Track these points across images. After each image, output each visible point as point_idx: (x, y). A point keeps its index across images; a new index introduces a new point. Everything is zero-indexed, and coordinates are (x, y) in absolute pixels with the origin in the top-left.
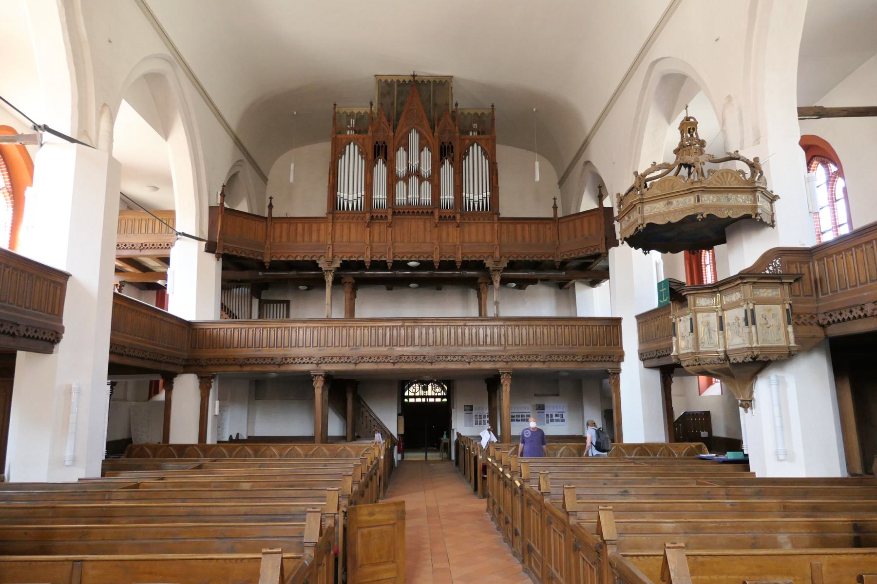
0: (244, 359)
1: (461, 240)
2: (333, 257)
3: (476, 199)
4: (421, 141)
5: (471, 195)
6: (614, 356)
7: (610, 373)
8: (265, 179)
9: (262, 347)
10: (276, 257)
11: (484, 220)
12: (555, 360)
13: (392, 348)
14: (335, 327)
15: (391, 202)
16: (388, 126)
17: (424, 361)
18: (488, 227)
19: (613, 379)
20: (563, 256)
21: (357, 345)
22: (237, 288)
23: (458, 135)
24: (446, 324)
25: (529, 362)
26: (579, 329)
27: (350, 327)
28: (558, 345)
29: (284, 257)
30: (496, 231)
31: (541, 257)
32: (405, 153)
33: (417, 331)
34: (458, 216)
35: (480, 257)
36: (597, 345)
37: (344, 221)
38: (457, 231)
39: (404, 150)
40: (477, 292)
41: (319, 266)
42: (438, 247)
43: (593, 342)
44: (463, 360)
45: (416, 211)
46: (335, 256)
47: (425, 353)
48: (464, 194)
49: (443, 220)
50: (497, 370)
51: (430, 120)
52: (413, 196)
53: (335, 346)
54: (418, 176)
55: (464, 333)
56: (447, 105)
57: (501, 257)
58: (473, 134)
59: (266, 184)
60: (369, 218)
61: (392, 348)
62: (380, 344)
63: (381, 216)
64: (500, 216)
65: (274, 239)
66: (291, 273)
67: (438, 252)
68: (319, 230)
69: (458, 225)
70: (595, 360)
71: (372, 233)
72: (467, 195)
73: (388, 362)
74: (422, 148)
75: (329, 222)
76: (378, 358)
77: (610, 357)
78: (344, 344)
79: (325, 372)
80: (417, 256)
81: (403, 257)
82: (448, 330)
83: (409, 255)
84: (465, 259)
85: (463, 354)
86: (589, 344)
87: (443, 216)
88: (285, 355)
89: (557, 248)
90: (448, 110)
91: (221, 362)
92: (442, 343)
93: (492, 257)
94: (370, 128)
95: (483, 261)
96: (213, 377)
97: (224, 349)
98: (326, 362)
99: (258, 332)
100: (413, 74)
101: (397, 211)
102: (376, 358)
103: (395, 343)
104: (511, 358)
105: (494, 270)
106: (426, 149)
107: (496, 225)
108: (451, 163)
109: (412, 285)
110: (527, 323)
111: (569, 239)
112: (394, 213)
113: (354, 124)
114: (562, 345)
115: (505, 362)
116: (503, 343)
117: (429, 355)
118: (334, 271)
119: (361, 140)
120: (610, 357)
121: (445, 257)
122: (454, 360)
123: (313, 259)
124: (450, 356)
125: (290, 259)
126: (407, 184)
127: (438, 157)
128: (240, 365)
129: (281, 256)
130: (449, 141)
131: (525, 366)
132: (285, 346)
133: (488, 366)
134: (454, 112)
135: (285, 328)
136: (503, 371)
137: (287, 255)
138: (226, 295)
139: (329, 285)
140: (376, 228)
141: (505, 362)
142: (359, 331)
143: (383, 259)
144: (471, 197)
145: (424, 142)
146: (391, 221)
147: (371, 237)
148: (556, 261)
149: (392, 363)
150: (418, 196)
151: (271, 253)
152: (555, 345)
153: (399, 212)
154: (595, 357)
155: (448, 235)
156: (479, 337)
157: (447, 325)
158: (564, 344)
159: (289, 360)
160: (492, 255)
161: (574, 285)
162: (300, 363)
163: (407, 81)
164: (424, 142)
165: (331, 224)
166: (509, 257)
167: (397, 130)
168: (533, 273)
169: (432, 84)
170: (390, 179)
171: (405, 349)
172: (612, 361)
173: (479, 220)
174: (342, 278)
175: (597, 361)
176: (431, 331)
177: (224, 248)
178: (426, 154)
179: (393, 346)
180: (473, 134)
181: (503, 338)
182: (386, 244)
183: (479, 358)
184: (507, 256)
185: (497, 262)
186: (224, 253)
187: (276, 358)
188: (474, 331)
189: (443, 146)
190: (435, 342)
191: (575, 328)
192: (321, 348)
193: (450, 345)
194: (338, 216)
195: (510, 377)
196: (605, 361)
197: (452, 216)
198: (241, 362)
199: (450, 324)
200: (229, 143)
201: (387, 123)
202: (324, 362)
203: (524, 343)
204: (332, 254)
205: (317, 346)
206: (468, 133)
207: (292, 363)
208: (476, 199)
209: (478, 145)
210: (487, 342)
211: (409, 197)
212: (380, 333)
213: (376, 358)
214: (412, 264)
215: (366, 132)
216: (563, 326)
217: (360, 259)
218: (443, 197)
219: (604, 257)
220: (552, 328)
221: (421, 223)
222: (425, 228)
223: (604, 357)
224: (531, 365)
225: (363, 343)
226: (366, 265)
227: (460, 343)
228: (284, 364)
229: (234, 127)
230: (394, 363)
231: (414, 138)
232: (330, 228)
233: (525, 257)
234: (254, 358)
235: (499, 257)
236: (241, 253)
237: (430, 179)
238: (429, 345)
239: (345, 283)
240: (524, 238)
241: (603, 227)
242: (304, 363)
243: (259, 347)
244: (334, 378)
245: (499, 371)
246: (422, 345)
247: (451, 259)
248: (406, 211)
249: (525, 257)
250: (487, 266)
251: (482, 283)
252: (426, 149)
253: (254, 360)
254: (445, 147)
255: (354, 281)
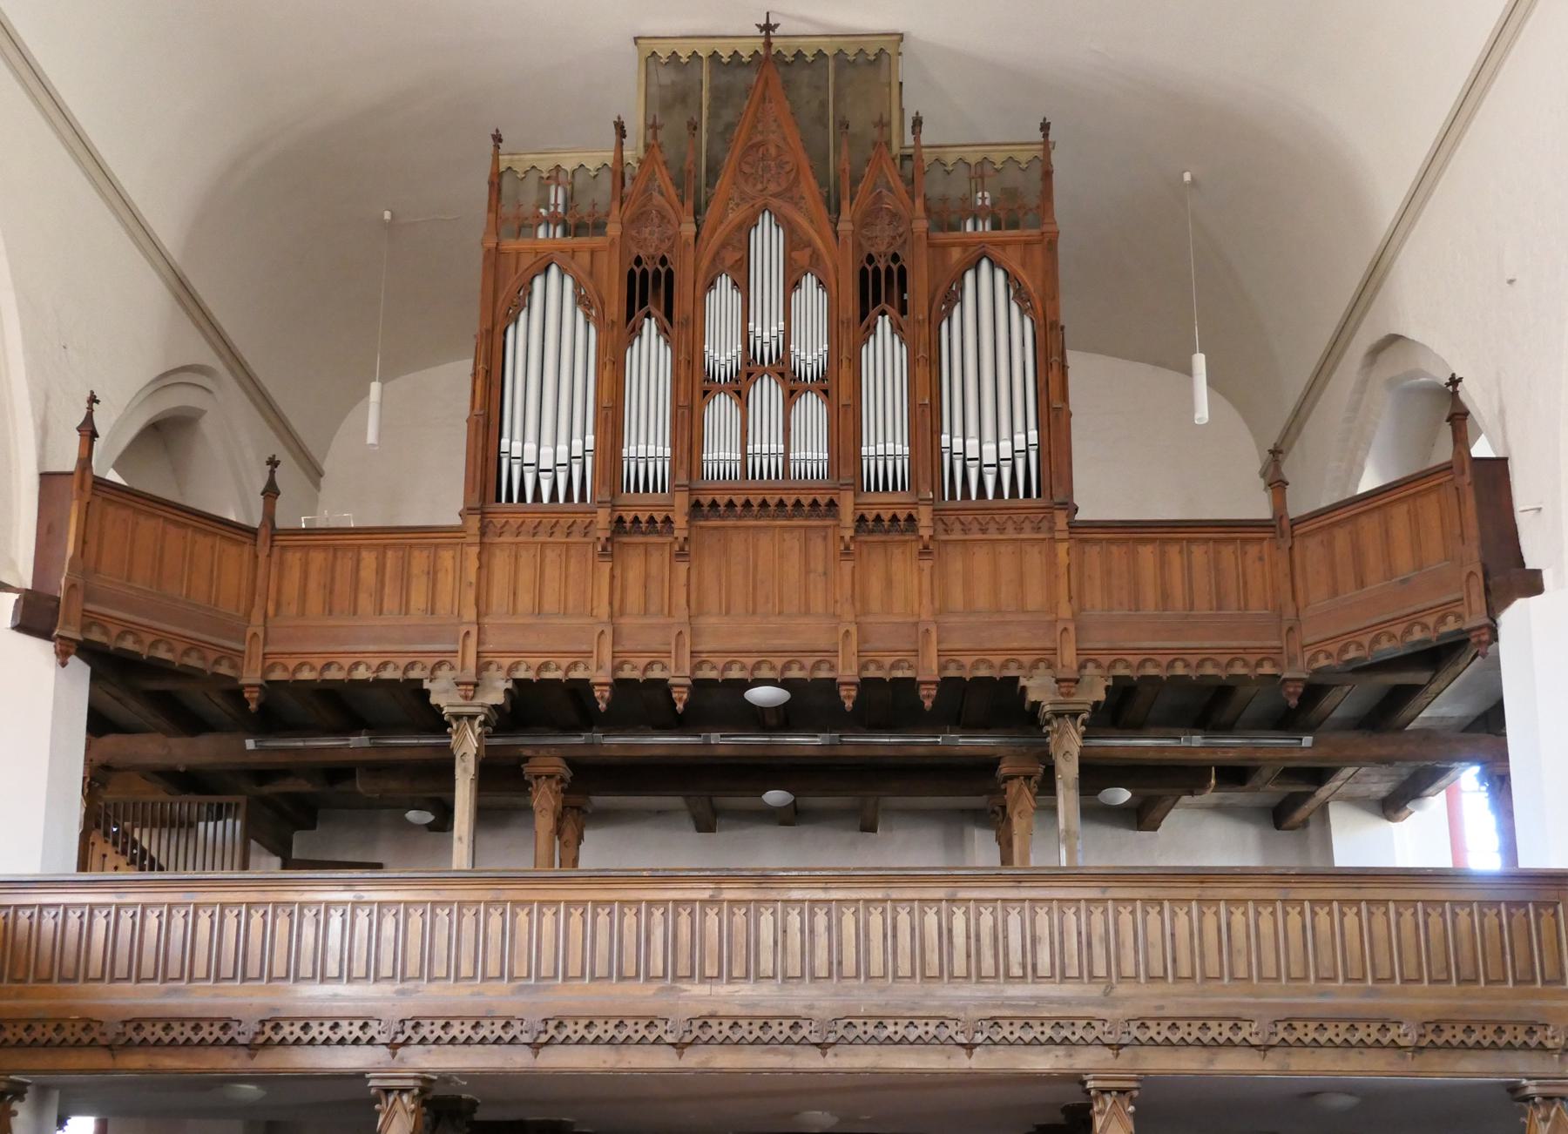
0: (125, 1023)
1: (937, 605)
2: (482, 667)
3: (989, 458)
4: (794, 254)
5: (972, 443)
6: (1546, 1026)
7: (1528, 1099)
8: (319, 473)
9: (191, 979)
10: (285, 669)
11: (1020, 530)
12: (1307, 1040)
13: (672, 988)
14: (461, 904)
15: (685, 466)
16: (677, 204)
17: (796, 1038)
18: (1035, 558)
19: (1546, 1119)
20: (1314, 658)
21: (543, 974)
22: (219, 818)
23: (921, 225)
24: (879, 895)
25: (1204, 1046)
26: (1399, 914)
27: (515, 903)
28: (1318, 979)
29: (312, 669)
30: (1063, 570)
31: (1230, 664)
32: (737, 298)
33: (766, 921)
34: (924, 516)
35: (1004, 666)
36: (1476, 981)
37: (520, 539)
38: (921, 570)
39: (735, 284)
40: (993, 834)
41: (433, 700)
42: (853, 629)
43: (1458, 969)
44: (944, 1034)
45: (772, 500)
46: (490, 663)
47: (797, 1009)
48: (945, 438)
49: (871, 532)
50: (1078, 1079)
51: (823, 183)
52: (765, 446)
53: (457, 979)
54: (782, 375)
55: (950, 931)
56: (883, 124)
57: (1082, 666)
58: (975, 228)
59: (317, 486)
60: (607, 526)
61: (672, 988)
62: (630, 970)
63: (652, 520)
64: (1078, 517)
65: (278, 605)
66: (354, 741)
67: (855, 649)
68: (433, 574)
69: (926, 547)
70: (1471, 1041)
71: (618, 582)
72: (958, 442)
73: (658, 1041)
74: (794, 279)
75: (469, 545)
76: (620, 1025)
77: (1530, 1032)
78: (493, 970)
79: (424, 1080)
80: (779, 662)
81: (728, 666)
82: (884, 921)
83: (750, 661)
84: (952, 672)
85: (949, 1014)
86: (1444, 976)
87: (871, 515)
88: (274, 1009)
89: (1291, 629)
90: (888, 144)
91: (37, 1033)
92: (862, 970)
93: (1050, 666)
94: (616, 212)
95: (1016, 679)
96: (18, 1092)
97: (55, 984)
98: (423, 1041)
99: (178, 921)
100: (763, 22)
101: (706, 500)
102: (611, 1026)
103: (683, 970)
104: (1135, 1032)
105: (1058, 715)
106: (809, 282)
107: (1062, 548)
108: (897, 328)
109: (775, 797)
110: (1195, 893)
111: (1335, 593)
112: (697, 505)
113: (560, 201)
114: (1334, 979)
115: (1109, 1046)
116: (1100, 970)
117: (815, 1013)
118: (482, 718)
119: (585, 258)
120: (1531, 1032)
121: (880, 667)
122: (912, 1038)
123: (414, 674)
124: (896, 1019)
125: (333, 674)
126: (744, 405)
127: (851, 306)
128: (108, 1047)
129: (302, 664)
130: (891, 251)
131: (1188, 1063)
132: (275, 974)
133: (1042, 1062)
134: (910, 156)
135: (276, 904)
136: (1100, 1084)
137: (324, 662)
138: (173, 842)
139: (465, 770)
140: (634, 568)
141: (1109, 1046)
142: (548, 920)
143: (656, 673)
144: (972, 452)
145: (803, 257)
146: (686, 534)
147: (617, 596)
148: (1286, 675)
149: (673, 1045)
150: (781, 448)
151: (264, 654)
152: (1306, 978)
153: (714, 504)
154: (1469, 1030)
155: (889, 583)
156: (1006, 948)
157: (884, 901)
158: (1341, 978)
159: (286, 1029)
160: (1047, 658)
161: (1323, 809)
162: (327, 1042)
163: (746, 56)
164: (803, 257)
165: (476, 549)
166: (1112, 665)
167: (710, 215)
168: (1197, 740)
169: (831, 64)
170: (682, 386)
171: (723, 989)
172: (1541, 1047)
173: (1002, 530)
174: (526, 759)
175: (1478, 1046)
176: (821, 921)
177: (89, 621)
178: (811, 300)
179: (676, 978)
180: (975, 228)
181: (1099, 950)
182: (671, 620)
183: (1005, 1032)
184: (1106, 660)
185: (1068, 683)
186: (87, 641)
187: (240, 1022)
188: (987, 921)
189: (870, 269)
190: (835, 968)
191: (1386, 913)
192: (407, 985)
193: (896, 977)
194: (499, 521)
195: (1131, 1109)
196: (1510, 1046)
197: (902, 515)
198: (111, 1036)
199: (895, 894)
200: (154, 293)
201: (672, 191)
202: (416, 1038)
203: (1185, 971)
204: (478, 657)
205: (393, 977)
206: (956, 227)
207: (298, 1042)
208: (989, 458)
209: (993, 265)
210: (1039, 967)
211: (750, 450)
212: (630, 926)
213: (611, 1026)
214: (761, 695)
215: (599, 227)
216: (1335, 905)
217: (575, 675)
218: (872, 449)
219: (1480, 643)
220: (1294, 913)
221: (793, 543)
222: (807, 563)
223: (1508, 1028)
224: (1211, 1061)
225: (565, 968)
226: (597, 694)
227: (933, 970)
228: (268, 1043)
229: (169, 237)
230: (679, 1046)
231: (767, 244)
232: (472, 564)
233: (1171, 665)
234: (160, 1019)
235: (1075, 667)
236: (154, 645)
237: (824, 386)
238: (814, 978)
239: (537, 777)
240: (1165, 597)
241: (1473, 531)
242: (342, 1041)
243: (181, 978)
244: (480, 1115)
245: (1084, 1083)
246: (786, 978)
247: (899, 674)
248: (739, 500)
249: (1171, 665)
250: (1032, 697)
251: (1012, 778)
252: (809, 282)
253: (159, 1026)
254: (877, 271)
255: (568, 774)
